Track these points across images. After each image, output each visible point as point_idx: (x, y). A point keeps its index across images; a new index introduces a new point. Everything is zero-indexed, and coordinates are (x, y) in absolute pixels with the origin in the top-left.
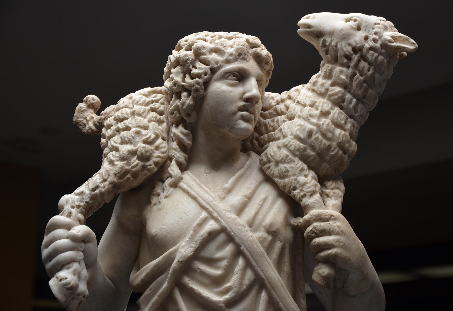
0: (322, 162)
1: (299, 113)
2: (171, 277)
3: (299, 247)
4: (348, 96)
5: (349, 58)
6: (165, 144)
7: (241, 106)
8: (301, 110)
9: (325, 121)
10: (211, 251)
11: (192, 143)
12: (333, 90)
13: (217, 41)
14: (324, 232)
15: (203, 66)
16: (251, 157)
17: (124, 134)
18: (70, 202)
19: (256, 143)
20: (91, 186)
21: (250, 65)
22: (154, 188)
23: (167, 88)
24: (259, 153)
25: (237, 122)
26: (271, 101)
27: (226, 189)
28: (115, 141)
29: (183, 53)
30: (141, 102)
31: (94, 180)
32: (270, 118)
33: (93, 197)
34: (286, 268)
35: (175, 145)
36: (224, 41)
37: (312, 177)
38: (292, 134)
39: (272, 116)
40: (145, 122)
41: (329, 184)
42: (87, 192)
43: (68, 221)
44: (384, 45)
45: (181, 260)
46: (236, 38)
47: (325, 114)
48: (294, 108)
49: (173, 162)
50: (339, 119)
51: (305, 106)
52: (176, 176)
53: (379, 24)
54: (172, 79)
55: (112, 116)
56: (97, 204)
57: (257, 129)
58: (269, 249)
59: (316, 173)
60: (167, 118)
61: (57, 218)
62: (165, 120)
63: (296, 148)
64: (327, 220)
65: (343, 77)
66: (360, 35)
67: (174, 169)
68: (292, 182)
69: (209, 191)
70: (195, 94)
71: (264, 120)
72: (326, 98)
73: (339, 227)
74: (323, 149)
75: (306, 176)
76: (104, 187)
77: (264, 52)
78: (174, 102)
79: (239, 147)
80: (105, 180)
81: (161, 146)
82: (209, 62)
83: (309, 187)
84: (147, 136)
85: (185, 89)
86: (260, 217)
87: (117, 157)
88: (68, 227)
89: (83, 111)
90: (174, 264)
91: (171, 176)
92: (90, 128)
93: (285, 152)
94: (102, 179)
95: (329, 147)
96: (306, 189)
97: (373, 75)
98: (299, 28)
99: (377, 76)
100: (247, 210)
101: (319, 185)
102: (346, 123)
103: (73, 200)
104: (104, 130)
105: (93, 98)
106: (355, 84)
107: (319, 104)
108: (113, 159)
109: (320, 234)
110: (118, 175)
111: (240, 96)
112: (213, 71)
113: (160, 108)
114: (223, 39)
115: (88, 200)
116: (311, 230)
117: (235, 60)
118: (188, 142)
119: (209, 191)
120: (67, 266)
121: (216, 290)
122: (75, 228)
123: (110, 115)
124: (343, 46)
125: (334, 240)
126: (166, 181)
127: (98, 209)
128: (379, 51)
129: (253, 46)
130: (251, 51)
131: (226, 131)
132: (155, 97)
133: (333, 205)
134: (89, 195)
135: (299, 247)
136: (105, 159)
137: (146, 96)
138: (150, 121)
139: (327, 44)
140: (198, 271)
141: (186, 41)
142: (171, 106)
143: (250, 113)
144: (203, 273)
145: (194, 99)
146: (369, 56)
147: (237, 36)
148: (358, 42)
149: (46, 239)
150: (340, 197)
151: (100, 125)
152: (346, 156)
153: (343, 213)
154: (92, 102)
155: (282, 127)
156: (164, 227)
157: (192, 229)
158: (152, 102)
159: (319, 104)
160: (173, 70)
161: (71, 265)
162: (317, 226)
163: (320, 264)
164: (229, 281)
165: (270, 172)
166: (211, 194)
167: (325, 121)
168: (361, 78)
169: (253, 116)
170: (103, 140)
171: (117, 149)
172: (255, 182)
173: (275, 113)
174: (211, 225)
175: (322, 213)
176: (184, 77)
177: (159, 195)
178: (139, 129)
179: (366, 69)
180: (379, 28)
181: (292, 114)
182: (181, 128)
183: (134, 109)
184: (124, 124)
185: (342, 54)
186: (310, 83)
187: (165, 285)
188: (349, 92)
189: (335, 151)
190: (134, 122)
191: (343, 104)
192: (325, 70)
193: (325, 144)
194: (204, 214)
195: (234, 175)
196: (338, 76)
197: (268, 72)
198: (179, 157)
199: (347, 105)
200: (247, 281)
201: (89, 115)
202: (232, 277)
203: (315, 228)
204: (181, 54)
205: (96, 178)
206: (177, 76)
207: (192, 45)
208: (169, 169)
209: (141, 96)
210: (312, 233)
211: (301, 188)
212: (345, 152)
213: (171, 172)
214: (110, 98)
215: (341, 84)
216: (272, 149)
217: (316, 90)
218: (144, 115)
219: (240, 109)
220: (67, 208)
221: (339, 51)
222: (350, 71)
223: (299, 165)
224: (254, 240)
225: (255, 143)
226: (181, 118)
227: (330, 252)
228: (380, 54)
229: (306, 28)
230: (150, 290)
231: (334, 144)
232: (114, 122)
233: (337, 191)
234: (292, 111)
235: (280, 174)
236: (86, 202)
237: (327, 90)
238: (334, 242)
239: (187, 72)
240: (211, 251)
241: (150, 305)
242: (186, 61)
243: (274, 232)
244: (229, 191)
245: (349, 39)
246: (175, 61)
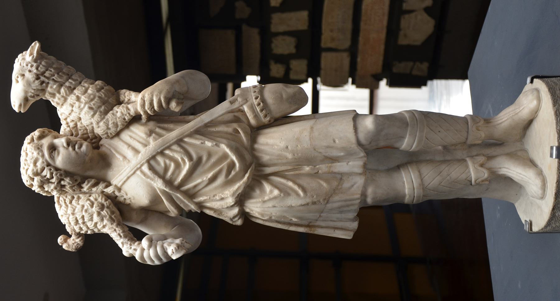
1: (77, 114)
2: (175, 192)
3: (159, 118)
4: (67, 84)
5: (43, 82)
6: (94, 195)
10: (160, 169)
13: (29, 162)
14: (151, 104)
17: (86, 219)
20: (119, 238)
21: (46, 142)
24: (101, 139)
26: (67, 130)
28: (90, 225)
30: (66, 210)
33: (125, 237)
34: (171, 126)
35: (94, 189)
39: (77, 130)
40: (79, 207)
41: (122, 98)
42: (122, 240)
43: (143, 251)
44: (35, 61)
47: (78, 99)
48: (74, 116)
49: (105, 190)
51: (72, 111)
54: (52, 190)
57: (85, 140)
58: (160, 136)
59: (115, 106)
61: (137, 257)
64: (144, 101)
65: (55, 87)
66: (27, 74)
67: (109, 190)
73: (148, 95)
75: (117, 112)
77: (36, 133)
80: (115, 230)
85: (59, 182)
86: (141, 140)
88: (143, 250)
89: (69, 245)
91: (114, 192)
92: (80, 241)
93: (101, 124)
95: (99, 97)
97: (54, 69)
98: (20, 112)
99: (54, 66)
100: (136, 147)
105: (60, 240)
108: (102, 226)
112: (48, 165)
114: (27, 159)
117: (42, 151)
118: (93, 181)
129: (32, 140)
130: (36, 141)
131: (87, 158)
133: (135, 97)
135: (159, 118)
137: (61, 206)
138: (78, 204)
141: (27, 181)
144: (173, 173)
145: (66, 177)
146: (42, 70)
149: (149, 263)
151: (79, 235)
158: (65, 203)
160: (46, 189)
168: (56, 75)
169: (78, 142)
170: (89, 232)
171: (96, 224)
174: (145, 168)
176: (52, 183)
177: (125, 199)
182: (84, 185)
187: (178, 195)
188: (64, 83)
190: (78, 214)
194: (138, 172)
196: (55, 89)
197: (49, 132)
203: (148, 109)
205: (114, 236)
212: (103, 88)
214: (61, 229)
216: (99, 131)
219: (74, 149)
220: (131, 251)
222: (51, 82)
225: (95, 141)
227: (163, 101)
228: (41, 63)
231: (97, 94)
232: (78, 226)
233: (126, 94)
234: (75, 119)
237: (63, 96)
239: (48, 181)
240: (160, 169)
241: (189, 204)
242: (41, 181)
244: (125, 157)
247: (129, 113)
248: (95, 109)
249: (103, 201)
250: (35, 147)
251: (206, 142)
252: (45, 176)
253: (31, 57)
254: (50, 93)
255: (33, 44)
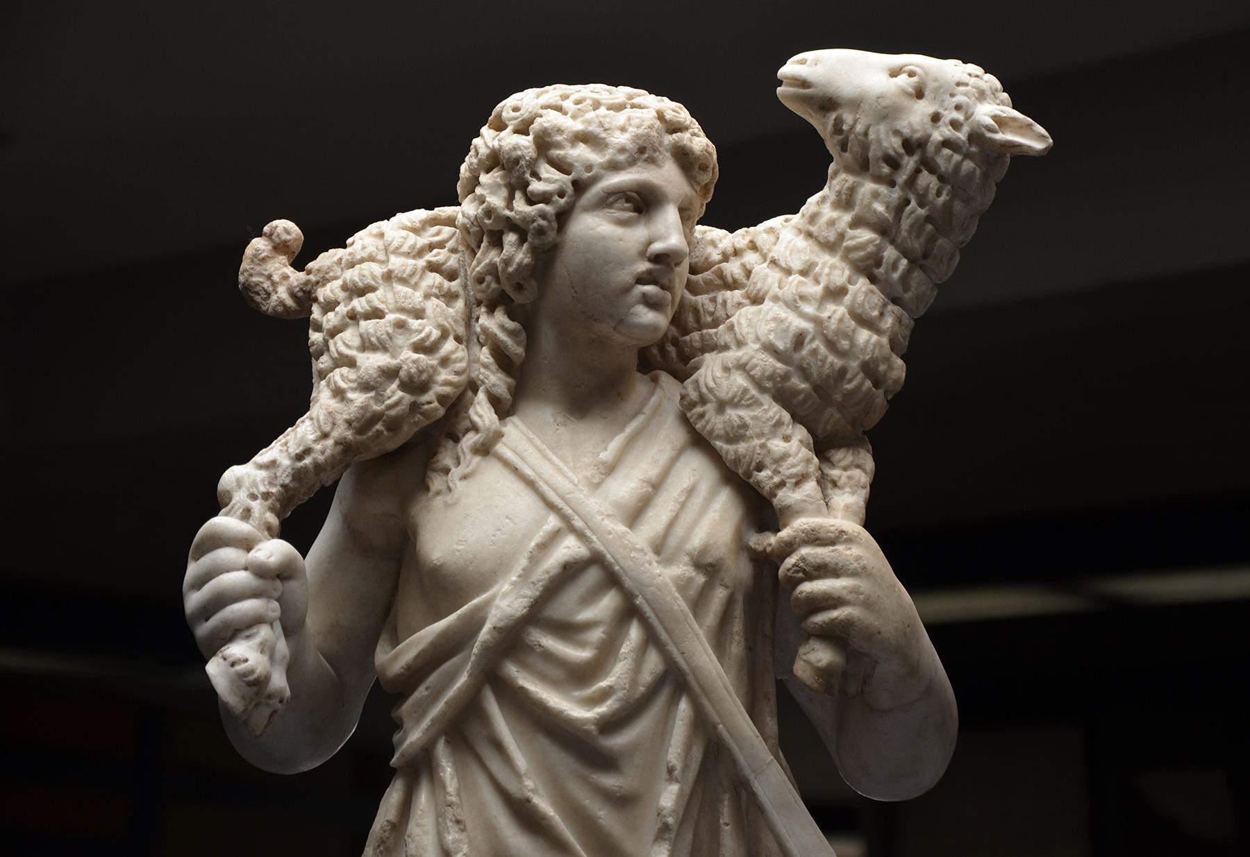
0: (820, 404)
2: (476, 664)
3: (766, 600)
4: (890, 253)
5: (894, 163)
6: (461, 353)
7: (643, 273)
8: (780, 282)
9: (834, 312)
10: (567, 606)
11: (526, 351)
12: (853, 238)
13: (590, 115)
15: (556, 175)
16: (661, 387)
17: (367, 326)
18: (247, 484)
19: (672, 349)
20: (294, 449)
21: (667, 176)
22: (435, 454)
23: (468, 218)
25: (633, 310)
26: (710, 249)
27: (603, 463)
29: (509, 140)
30: (405, 249)
31: (299, 436)
32: (706, 292)
33: (298, 475)
34: (736, 647)
35: (485, 355)
36: (605, 116)
37: (801, 441)
38: (758, 339)
39: (710, 287)
40: (417, 297)
41: (838, 455)
42: (286, 462)
43: (241, 539)
44: (976, 137)
45: (502, 624)
46: (633, 106)
47: (835, 293)
49: (481, 396)
50: (867, 306)
51: (789, 272)
52: (489, 429)
53: (967, 85)
54: (482, 200)
55: (336, 278)
56: (303, 490)
57: (676, 320)
58: (698, 604)
60: (465, 287)
61: (222, 522)
62: (461, 292)
63: (767, 374)
64: (832, 542)
65: (879, 208)
67: (481, 412)
68: (753, 452)
69: (565, 469)
70: (537, 241)
71: (693, 298)
72: (839, 254)
73: (858, 558)
74: (828, 376)
75: (787, 439)
76: (323, 453)
77: (699, 142)
78: (484, 254)
79: (634, 361)
80: (325, 436)
81: (454, 356)
82: (571, 165)
83: (794, 466)
84: (423, 335)
85: (512, 225)
86: (679, 531)
87: (352, 381)
88: (247, 544)
89: (264, 260)
90: (484, 634)
91: (475, 428)
92: (282, 303)
93: (740, 380)
94: (319, 433)
95: (842, 372)
96: (787, 469)
97: (948, 206)
98: (780, 83)
99: (958, 206)
100: (651, 513)
101: (816, 460)
102: (882, 314)
103: (254, 480)
104: (316, 309)
105: (285, 228)
106: (905, 224)
107: (822, 269)
108: (343, 385)
109: (815, 573)
110: (355, 424)
111: (642, 248)
112: (580, 187)
113: (449, 263)
114: (602, 111)
115: (287, 481)
116: (795, 565)
117: (632, 163)
118: (516, 349)
119: (565, 469)
120: (247, 633)
121: (577, 693)
122: (260, 546)
123: (331, 274)
124: (882, 136)
125: (844, 588)
126: (464, 440)
127: (306, 498)
128: (964, 150)
130: (669, 139)
131: (605, 328)
132: (437, 234)
133: (847, 508)
134: (289, 470)
135: (766, 600)
136: (323, 383)
137: (416, 231)
138: (427, 296)
139: (845, 128)
140: (539, 650)
141: (516, 109)
142: (479, 263)
143: (663, 287)
144: (548, 656)
145: (534, 250)
146: (940, 161)
147: (634, 101)
148: (917, 127)
150: (864, 487)
151: (305, 297)
152: (881, 392)
153: (867, 525)
154: (285, 237)
155: (733, 319)
156: (460, 547)
157: (527, 554)
158: (431, 247)
159: (822, 269)
160: (484, 178)
161: (254, 630)
162: (808, 554)
163: (811, 641)
164: (607, 675)
165: (705, 427)
166: (570, 474)
167: (834, 312)
168: (922, 212)
169: (669, 296)
170: (315, 337)
171: (351, 363)
172: (669, 447)
173: (719, 282)
174: (569, 548)
175: (821, 527)
176: (510, 199)
177: (447, 471)
178: (403, 317)
179: (933, 191)
180: (965, 94)
181: (759, 291)
182: (500, 317)
183: (390, 267)
184: (368, 302)
185: (880, 154)
186: (803, 215)
187: (463, 679)
188: (892, 242)
189: (856, 382)
191: (876, 271)
192: (837, 188)
193: (832, 365)
194: (553, 522)
195: (622, 430)
196: (869, 206)
197: (705, 188)
198: (494, 385)
199: (886, 273)
200: (647, 677)
201: (277, 269)
202: (614, 665)
203: (803, 559)
204: (503, 143)
205: (303, 431)
206: (493, 193)
207: (530, 121)
208: (471, 412)
209: (404, 233)
210: (797, 572)
211: (774, 467)
212: (877, 384)
213: (476, 418)
214: (326, 232)
215: (875, 224)
216: (712, 371)
217: (815, 234)
218: (413, 281)
219: (641, 280)
220: (240, 498)
221: (873, 147)
222: (896, 194)
223: (771, 413)
224: (666, 585)
225: (672, 355)
226: (500, 294)
227: (835, 614)
228: (967, 156)
229: (798, 86)
230: (427, 689)
231: (854, 364)
232: (341, 295)
233: (856, 473)
235: (727, 433)
236: (282, 486)
237: (842, 236)
238: (845, 592)
240: (567, 606)
241: (426, 722)
242: (517, 161)
243: (711, 565)
244: (610, 469)
245: (896, 119)
246: (489, 156)
247: (782, 484)
248: (797, 356)
249: (438, 389)
250: (648, 136)
251: (674, 788)
252: (536, 175)
253: (990, 122)
254: (852, 190)
255: (1041, 129)
